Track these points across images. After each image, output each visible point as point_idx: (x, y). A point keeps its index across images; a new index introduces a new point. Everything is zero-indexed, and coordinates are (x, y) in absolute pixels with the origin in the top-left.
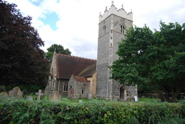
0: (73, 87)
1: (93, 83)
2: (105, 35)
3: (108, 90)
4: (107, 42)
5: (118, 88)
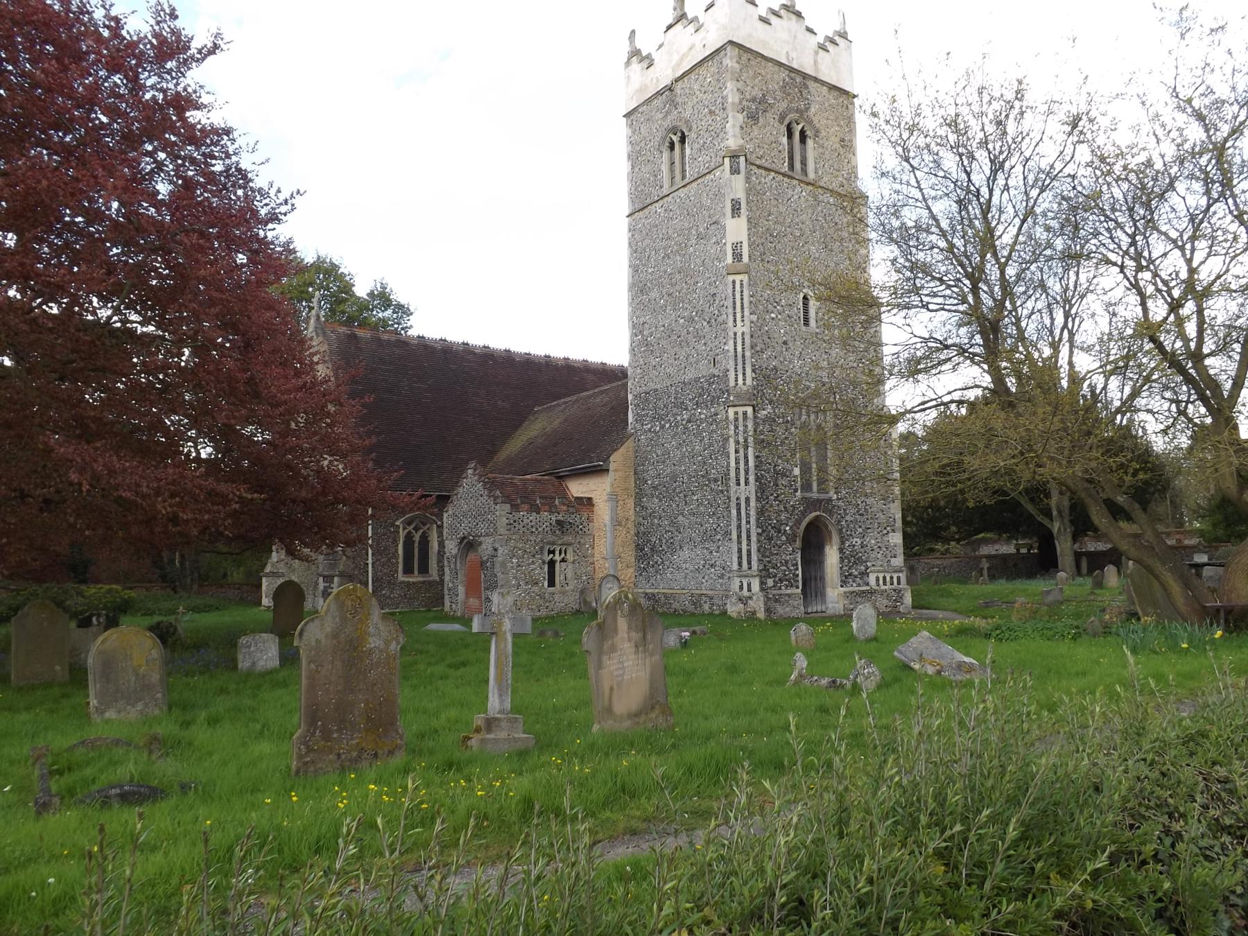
0: (486, 546)
1: (614, 511)
2: (682, 193)
3: (740, 551)
4: (700, 237)
5: (791, 539)
